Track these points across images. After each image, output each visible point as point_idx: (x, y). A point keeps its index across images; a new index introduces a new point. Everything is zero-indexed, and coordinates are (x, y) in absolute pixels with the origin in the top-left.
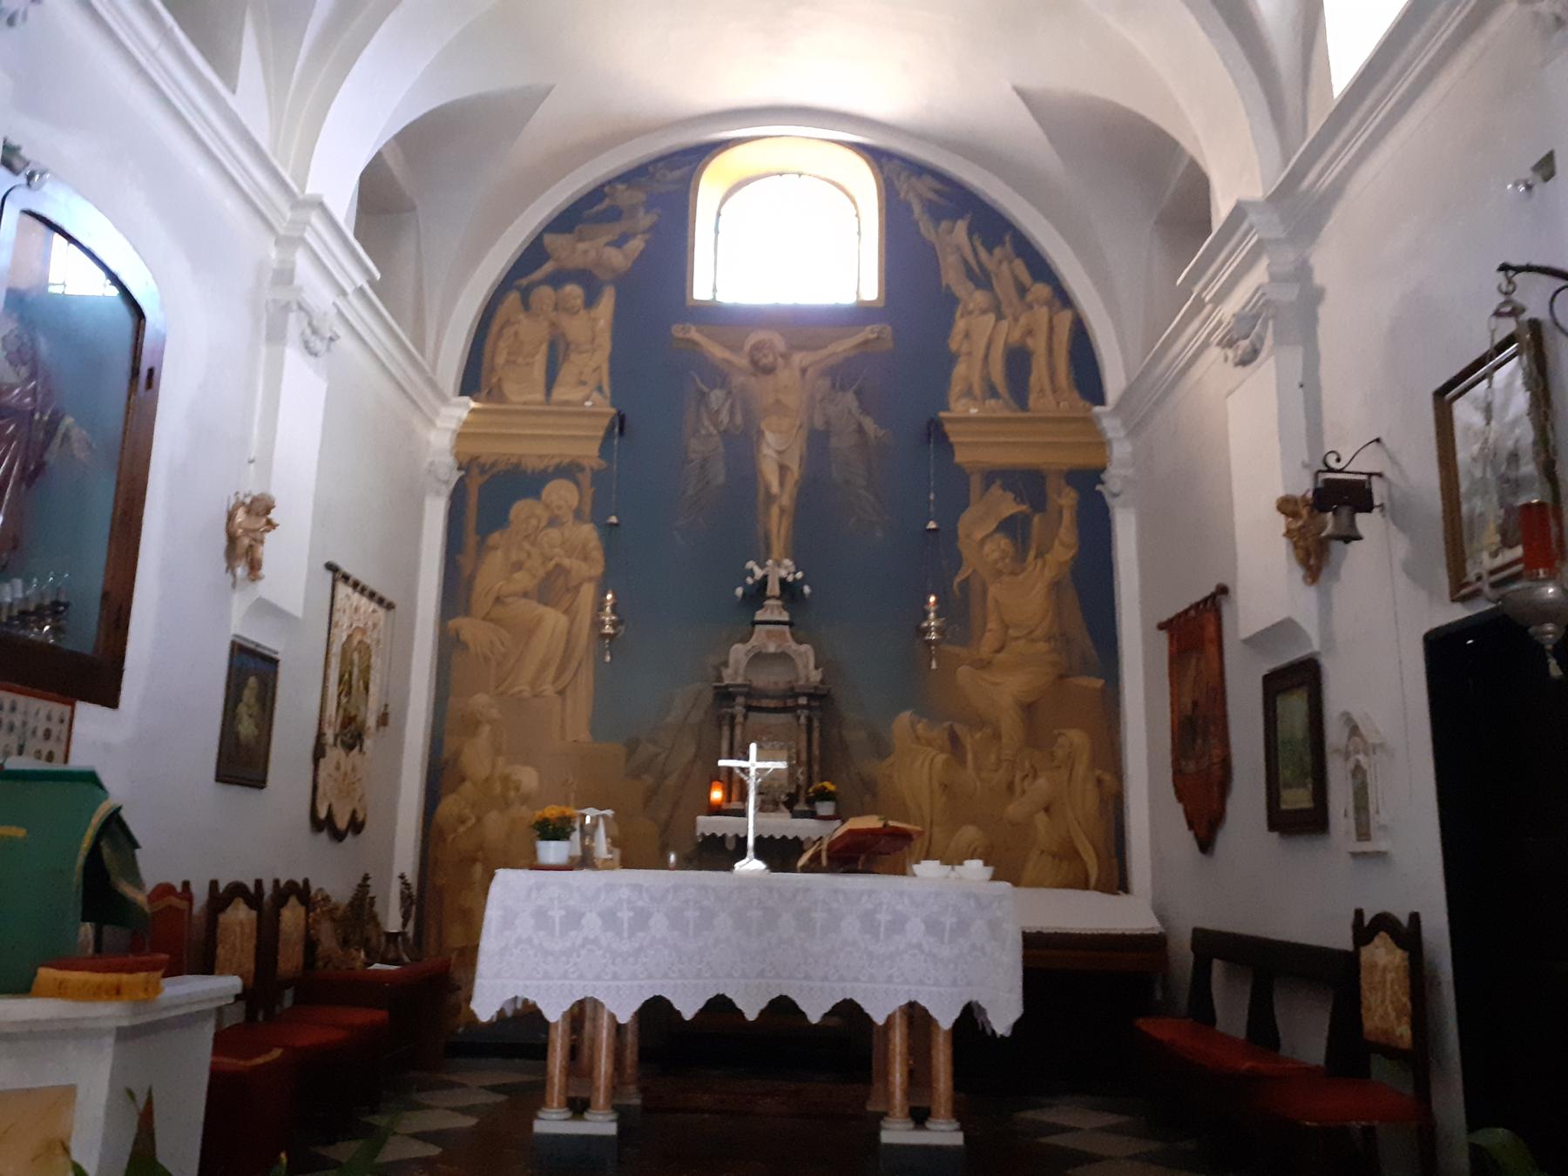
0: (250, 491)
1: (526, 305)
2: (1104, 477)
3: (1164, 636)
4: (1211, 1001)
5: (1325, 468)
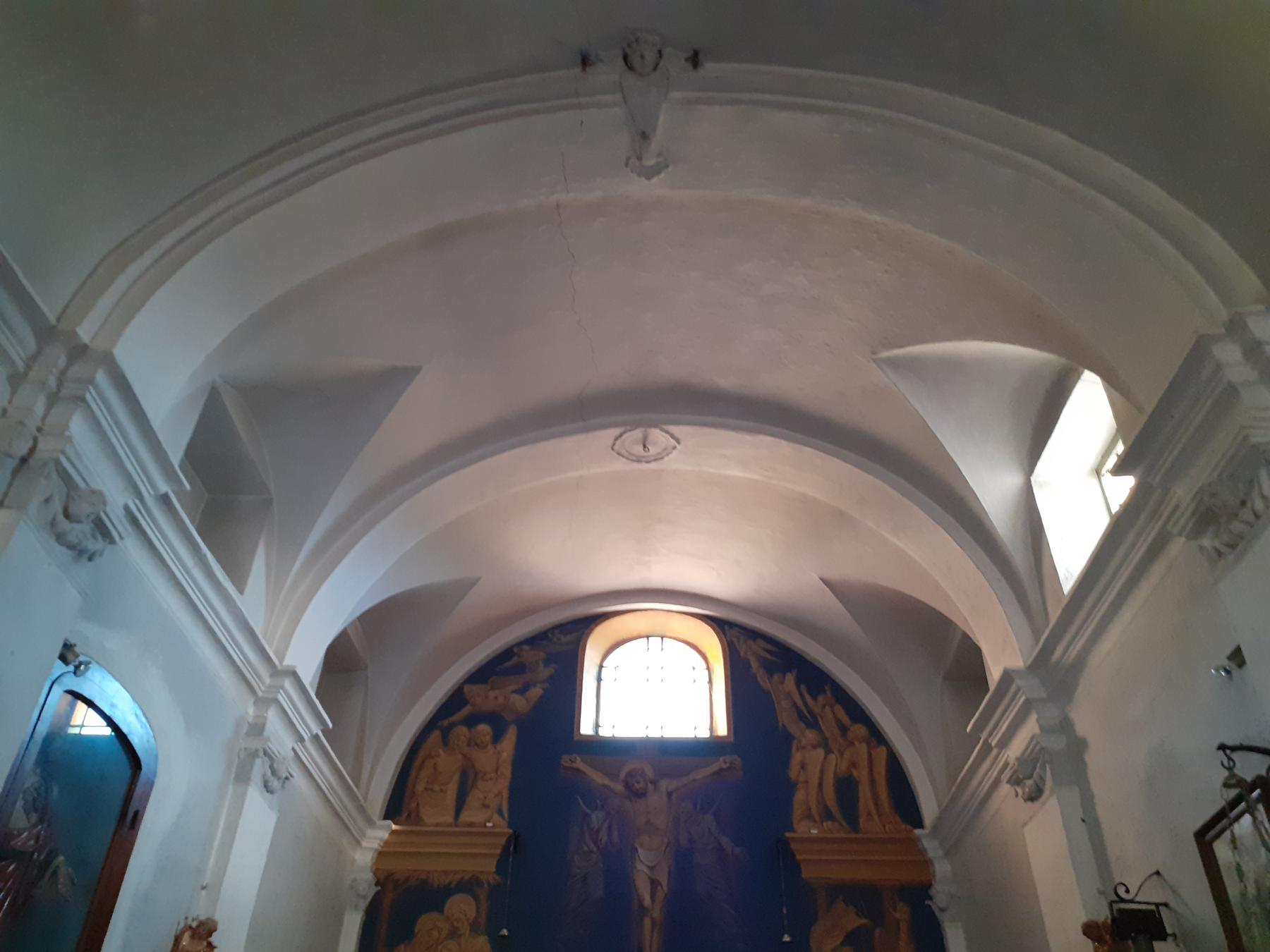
0: (198, 915)
1: (445, 741)
2: (932, 892)
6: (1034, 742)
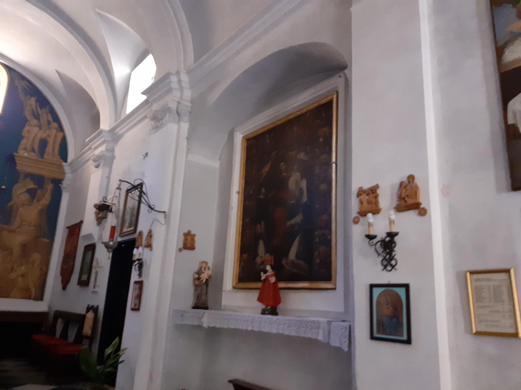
3: (67, 230)
4: (114, 340)
5: (103, 201)
6: (102, 152)
